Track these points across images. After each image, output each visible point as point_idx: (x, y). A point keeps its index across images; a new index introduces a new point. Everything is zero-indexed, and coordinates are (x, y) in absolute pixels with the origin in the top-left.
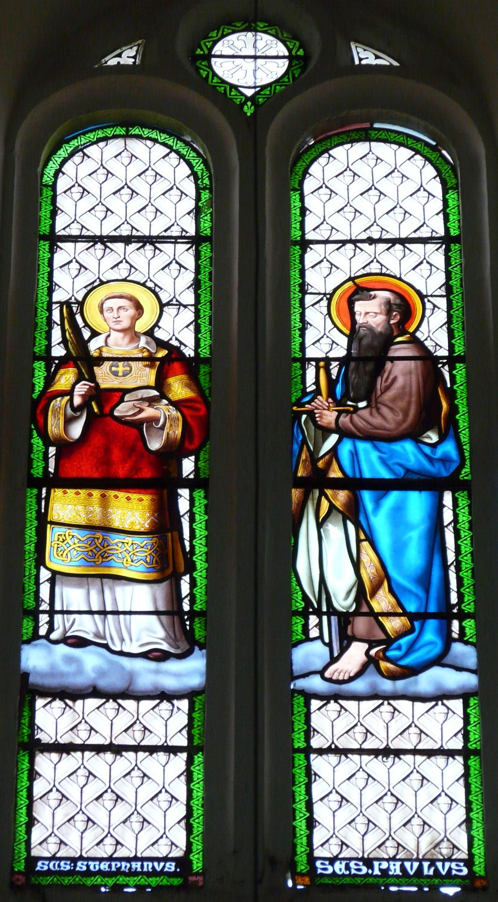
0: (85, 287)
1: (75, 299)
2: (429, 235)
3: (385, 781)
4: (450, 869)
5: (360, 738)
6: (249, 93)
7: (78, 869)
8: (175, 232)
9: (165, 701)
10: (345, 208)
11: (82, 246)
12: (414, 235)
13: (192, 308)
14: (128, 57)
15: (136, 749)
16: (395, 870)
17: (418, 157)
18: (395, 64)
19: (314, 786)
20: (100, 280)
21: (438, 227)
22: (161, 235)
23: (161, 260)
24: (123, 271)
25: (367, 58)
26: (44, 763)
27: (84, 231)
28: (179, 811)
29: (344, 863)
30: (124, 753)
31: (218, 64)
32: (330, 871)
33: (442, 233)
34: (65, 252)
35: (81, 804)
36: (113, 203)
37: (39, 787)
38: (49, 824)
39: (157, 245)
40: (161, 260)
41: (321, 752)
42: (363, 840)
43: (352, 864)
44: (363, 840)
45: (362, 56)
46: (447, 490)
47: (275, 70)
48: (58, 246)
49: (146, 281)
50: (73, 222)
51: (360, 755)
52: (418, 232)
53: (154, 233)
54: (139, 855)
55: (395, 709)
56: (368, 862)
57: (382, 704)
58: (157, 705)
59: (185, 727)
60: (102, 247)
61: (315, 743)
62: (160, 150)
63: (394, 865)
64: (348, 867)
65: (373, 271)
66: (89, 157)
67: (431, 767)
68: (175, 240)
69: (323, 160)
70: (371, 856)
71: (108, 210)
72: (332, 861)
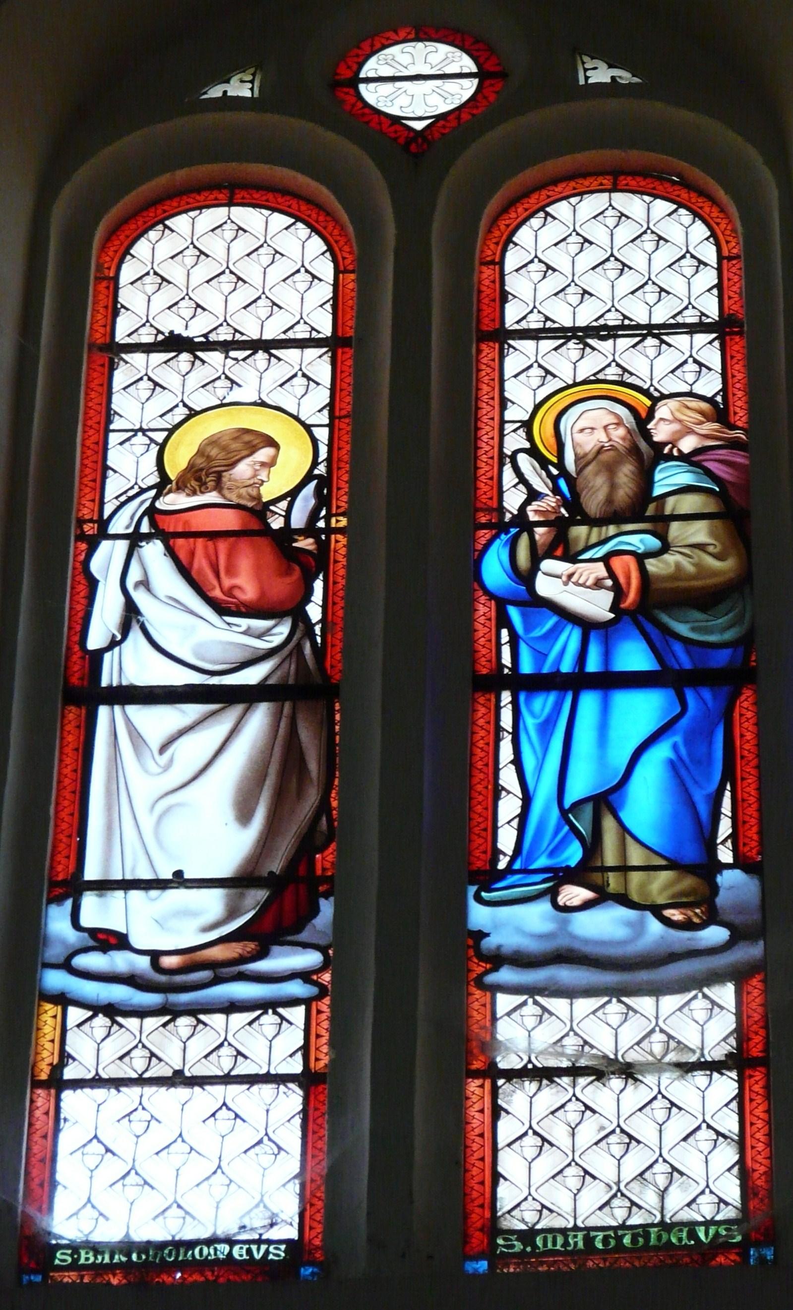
2: (306, 335)
3: (619, 1116)
5: (658, 1049)
6: (419, 126)
7: (82, 1261)
8: (690, 317)
9: (101, 1015)
11: (547, 345)
12: (672, 321)
15: (227, 1079)
17: (682, 211)
19: (502, 1125)
23: (278, 372)
24: (612, 373)
27: (238, 336)
30: (556, 1079)
35: (573, 1151)
37: (506, 1129)
38: (522, 1181)
40: (278, 372)
42: (575, 1200)
44: (575, 1200)
47: (466, 89)
48: (510, 346)
50: (531, 312)
53: (267, 336)
54: (580, 1224)
55: (713, 1003)
57: (525, 1003)
58: (603, 1006)
59: (731, 1033)
60: (266, 356)
61: (69, 1073)
62: (280, 220)
65: (610, 378)
66: (554, 218)
67: (685, 1090)
68: (693, 329)
69: (535, 222)
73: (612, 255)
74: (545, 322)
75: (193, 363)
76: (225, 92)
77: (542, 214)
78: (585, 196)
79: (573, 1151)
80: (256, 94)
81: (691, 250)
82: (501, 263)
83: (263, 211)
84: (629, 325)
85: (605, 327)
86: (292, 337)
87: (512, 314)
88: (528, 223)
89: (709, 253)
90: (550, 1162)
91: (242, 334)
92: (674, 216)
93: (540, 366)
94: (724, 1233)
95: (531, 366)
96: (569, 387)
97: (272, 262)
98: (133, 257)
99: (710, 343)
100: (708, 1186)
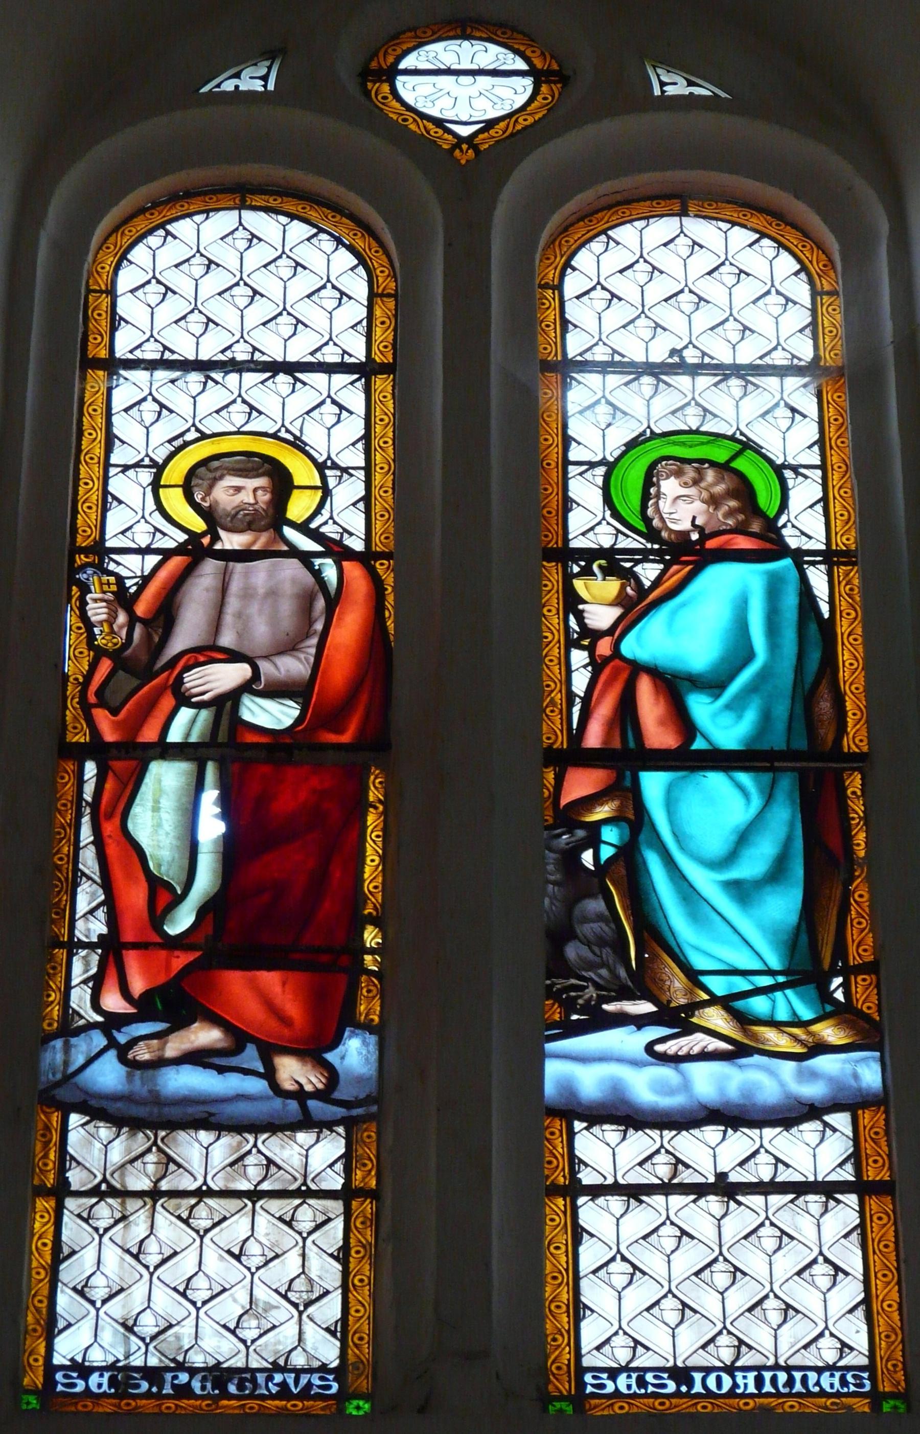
0: (170, 441)
1: (151, 460)
3: (702, 1240)
4: (309, 1384)
6: (465, 131)
10: (637, 321)
12: (221, 357)
13: (361, 474)
14: (251, 78)
16: (746, 1385)
17: (766, 242)
18: (723, 95)
20: (652, 432)
21: (805, 350)
22: (215, 358)
23: (304, 398)
25: (675, 84)
26: (590, 1213)
28: (850, 1291)
29: (838, 1374)
30: (644, 1198)
31: (409, 86)
32: (610, 1387)
33: (359, 353)
34: (128, 389)
35: (670, 1282)
36: (220, 310)
37: (590, 1255)
39: (298, 375)
40: (304, 398)
41: (596, 1191)
43: (649, 1377)
45: (665, 79)
46: (93, 759)
47: (516, 93)
48: (572, 378)
49: (279, 430)
51: (667, 1195)
52: (318, 355)
53: (292, 358)
54: (782, 1362)
56: (681, 1374)
62: (741, 236)
63: (745, 1377)
64: (844, 1382)
66: (175, 237)
68: (781, 372)
69: (597, 246)
70: (689, 1363)
71: (299, 321)
72: (613, 1374)
73: (599, 283)
74: (792, 360)
75: (205, 384)
76: (237, 87)
77: (161, 232)
78: (651, 220)
79: (670, 1282)
80: (271, 87)
81: (602, 281)
82: (559, 288)
83: (721, 224)
84: (709, 364)
85: (233, 361)
86: (770, 362)
87: (575, 345)
88: (587, 246)
89: (358, 286)
90: (642, 1293)
91: (173, 352)
92: (755, 247)
93: (155, 400)
94: (318, 1382)
95: (322, 403)
96: (690, 432)
97: (650, 280)
98: (131, 263)
99: (352, 383)
100: (827, 1328)
